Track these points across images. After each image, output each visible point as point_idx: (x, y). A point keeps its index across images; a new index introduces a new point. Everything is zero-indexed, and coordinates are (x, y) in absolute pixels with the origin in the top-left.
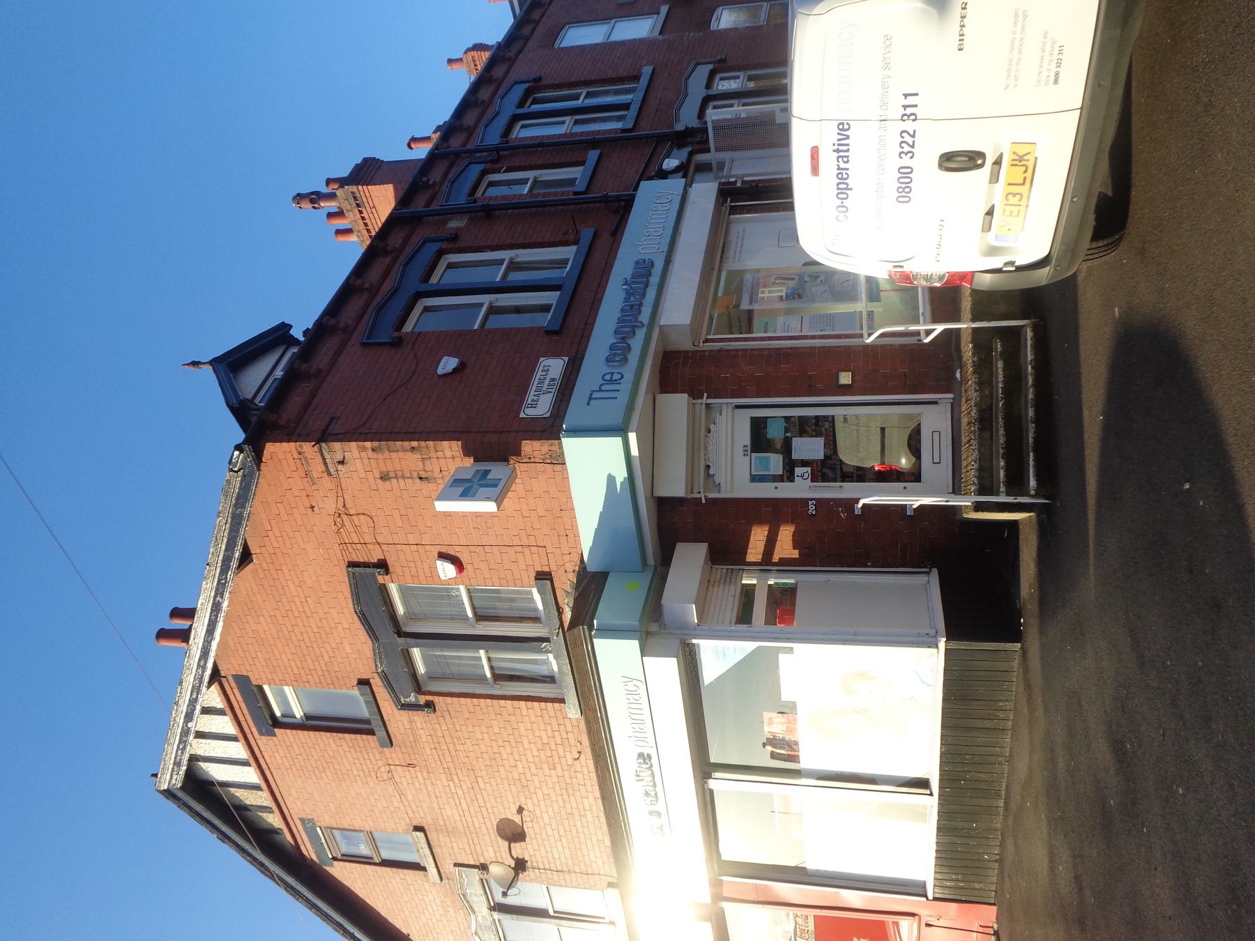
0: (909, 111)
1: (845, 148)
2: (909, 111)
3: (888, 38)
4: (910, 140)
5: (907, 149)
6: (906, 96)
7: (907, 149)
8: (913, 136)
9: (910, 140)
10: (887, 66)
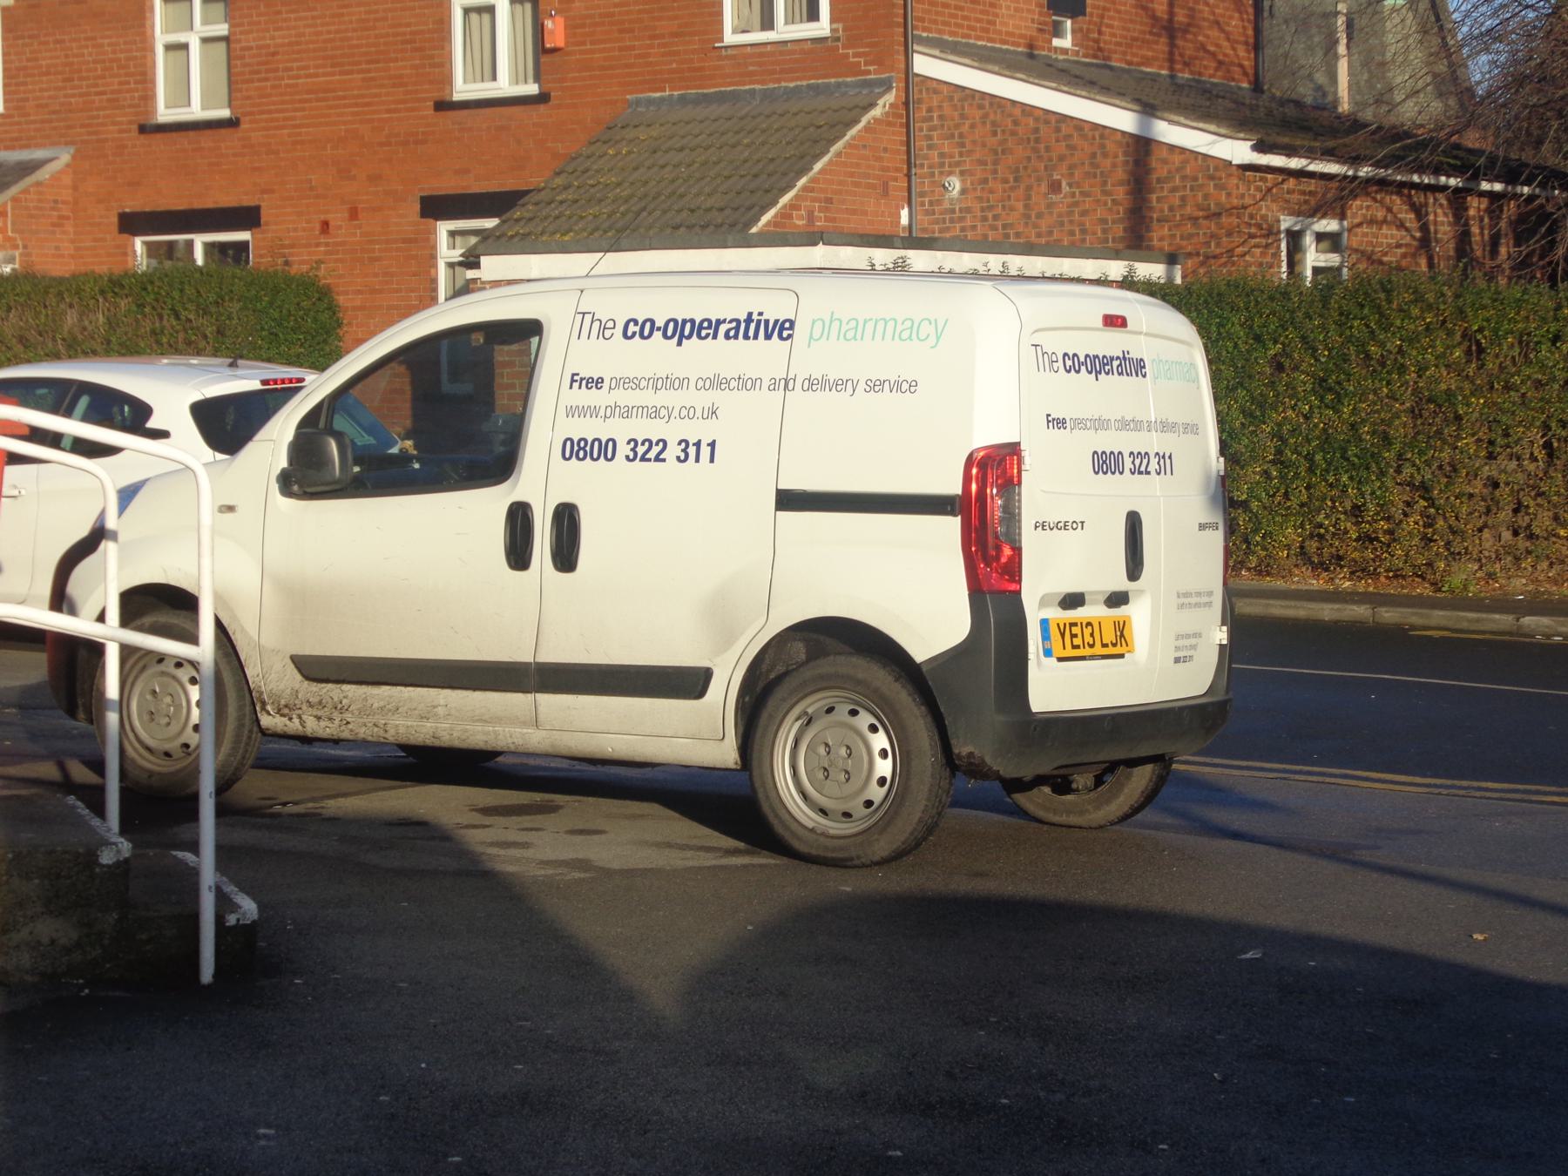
0: (692, 450)
1: (751, 333)
2: (692, 450)
3: (913, 385)
4: (651, 455)
5: (641, 450)
6: (712, 445)
7: (641, 450)
8: (657, 459)
9: (651, 455)
10: (875, 386)
